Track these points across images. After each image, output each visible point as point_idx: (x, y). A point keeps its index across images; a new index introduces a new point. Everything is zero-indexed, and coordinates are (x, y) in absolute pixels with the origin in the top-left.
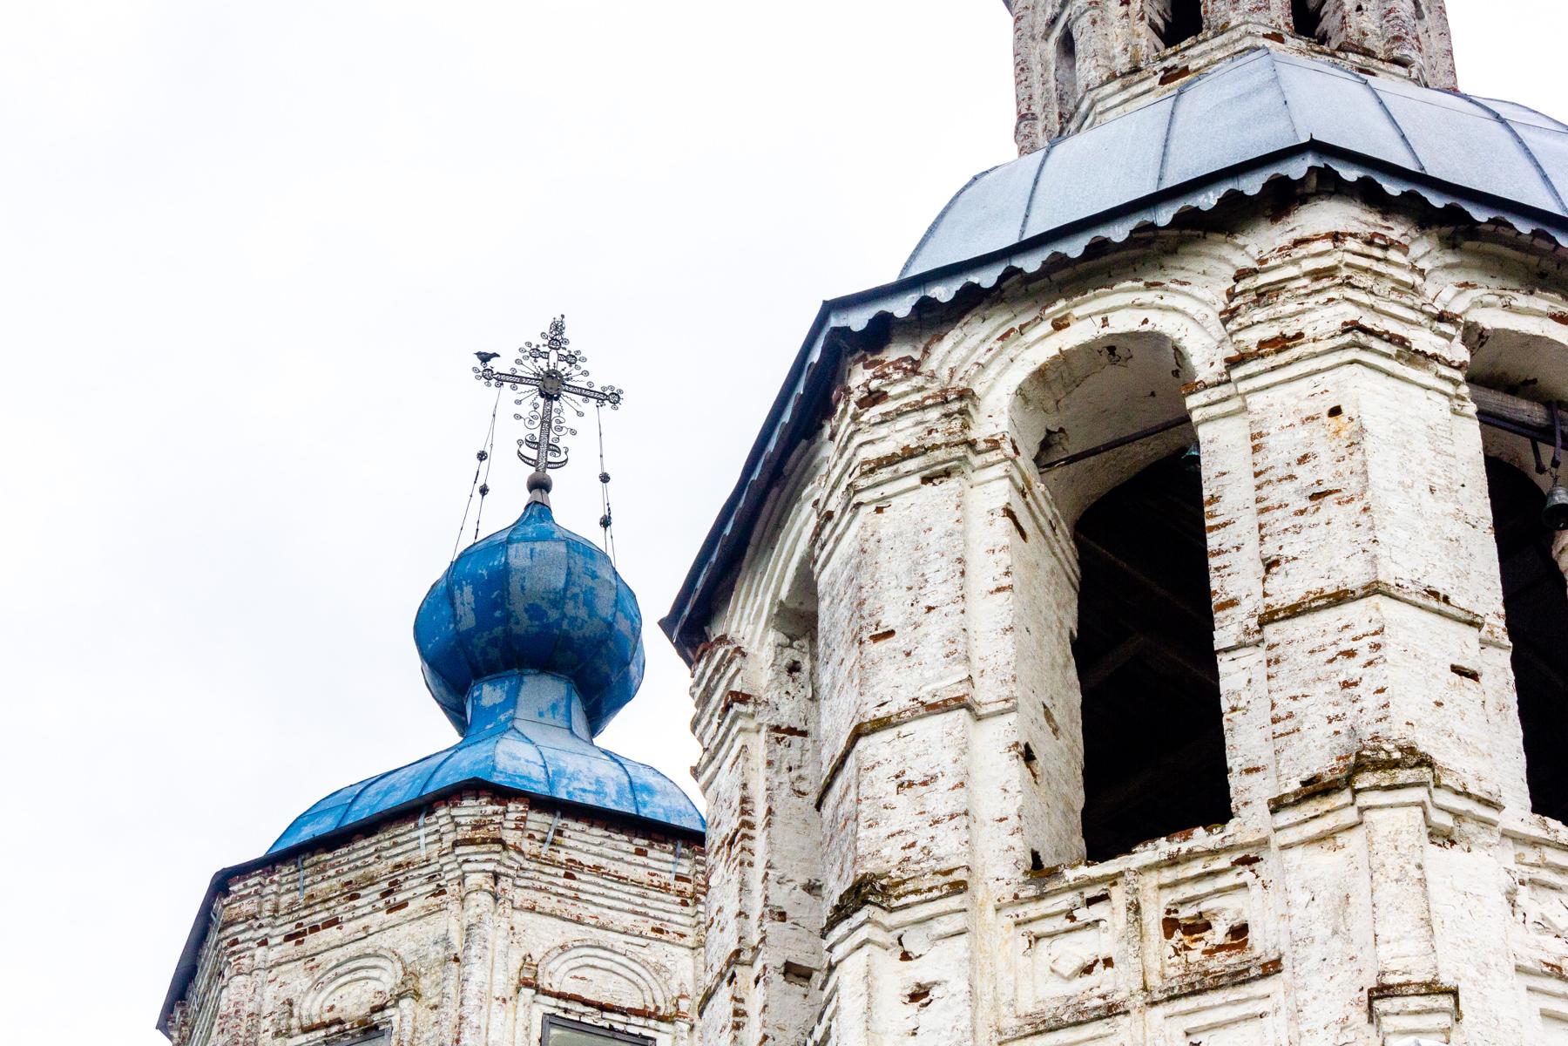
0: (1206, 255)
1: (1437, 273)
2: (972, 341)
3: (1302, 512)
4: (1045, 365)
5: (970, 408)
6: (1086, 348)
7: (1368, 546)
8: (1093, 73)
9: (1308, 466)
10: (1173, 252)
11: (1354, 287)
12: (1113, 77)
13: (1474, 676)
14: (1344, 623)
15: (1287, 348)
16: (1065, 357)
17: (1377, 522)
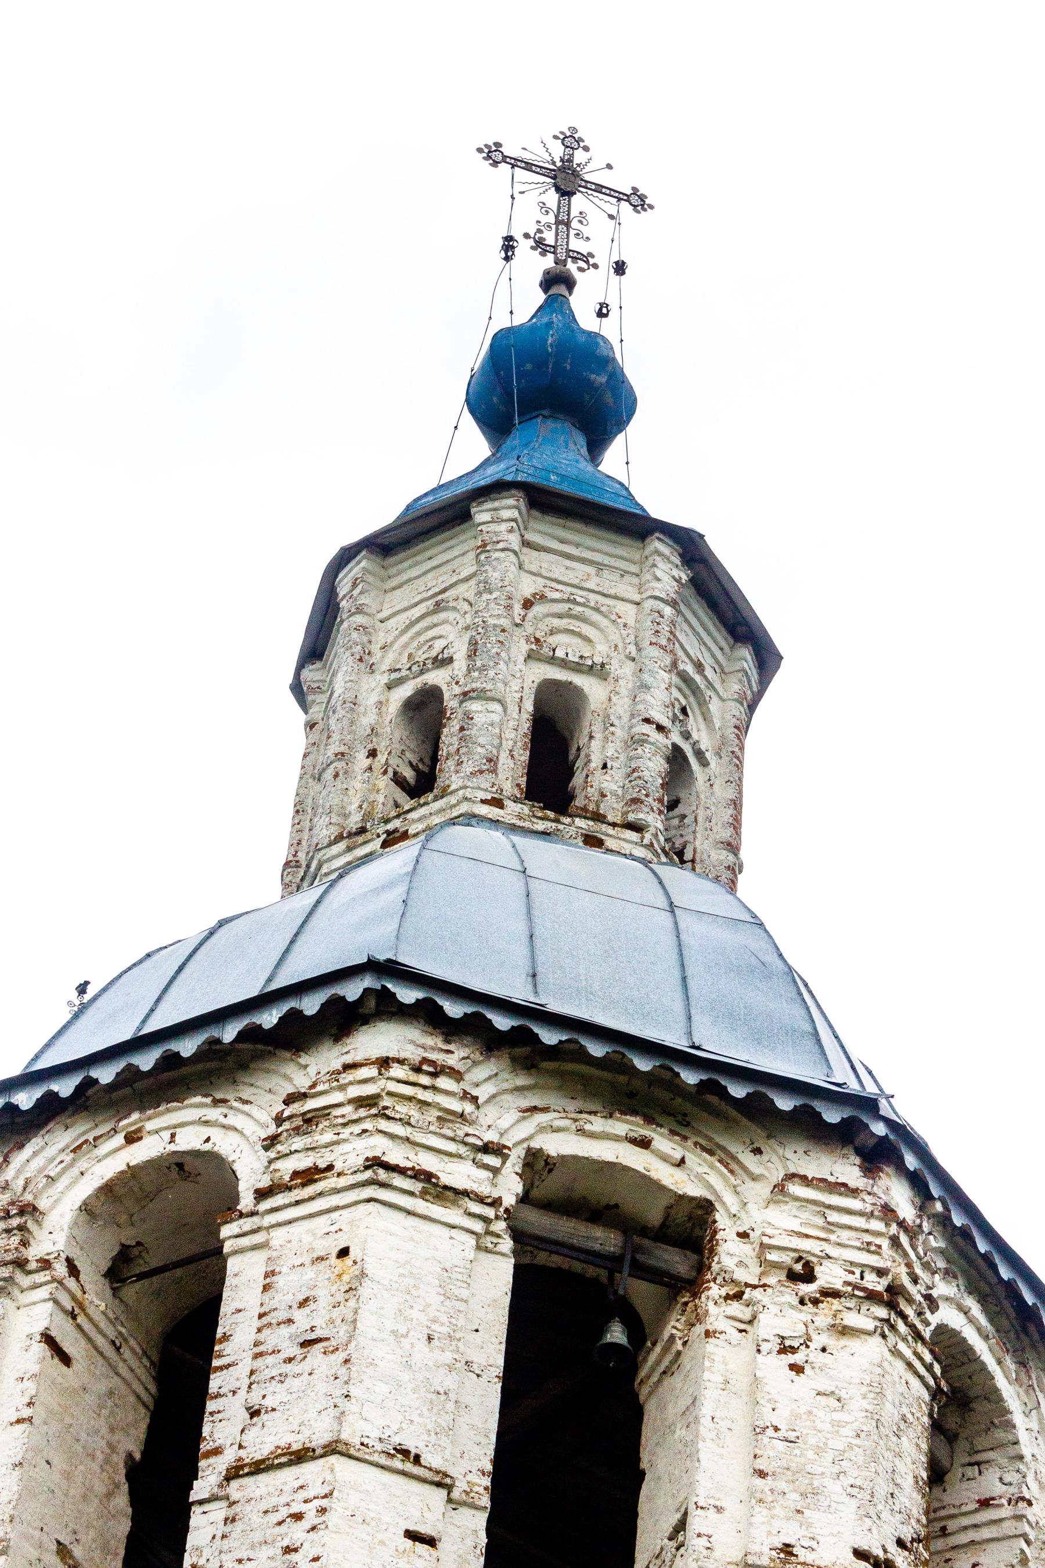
0: (274, 1072)
1: (505, 1097)
2: (51, 1151)
3: (290, 1360)
4: (111, 1180)
5: (30, 1225)
6: (151, 1164)
7: (339, 1401)
8: (325, 832)
9: (307, 1310)
10: (244, 1066)
11: (389, 1118)
12: (339, 838)
13: (430, 1542)
14: (300, 1483)
15: (316, 1181)
16: (132, 1173)
17: (354, 1375)
